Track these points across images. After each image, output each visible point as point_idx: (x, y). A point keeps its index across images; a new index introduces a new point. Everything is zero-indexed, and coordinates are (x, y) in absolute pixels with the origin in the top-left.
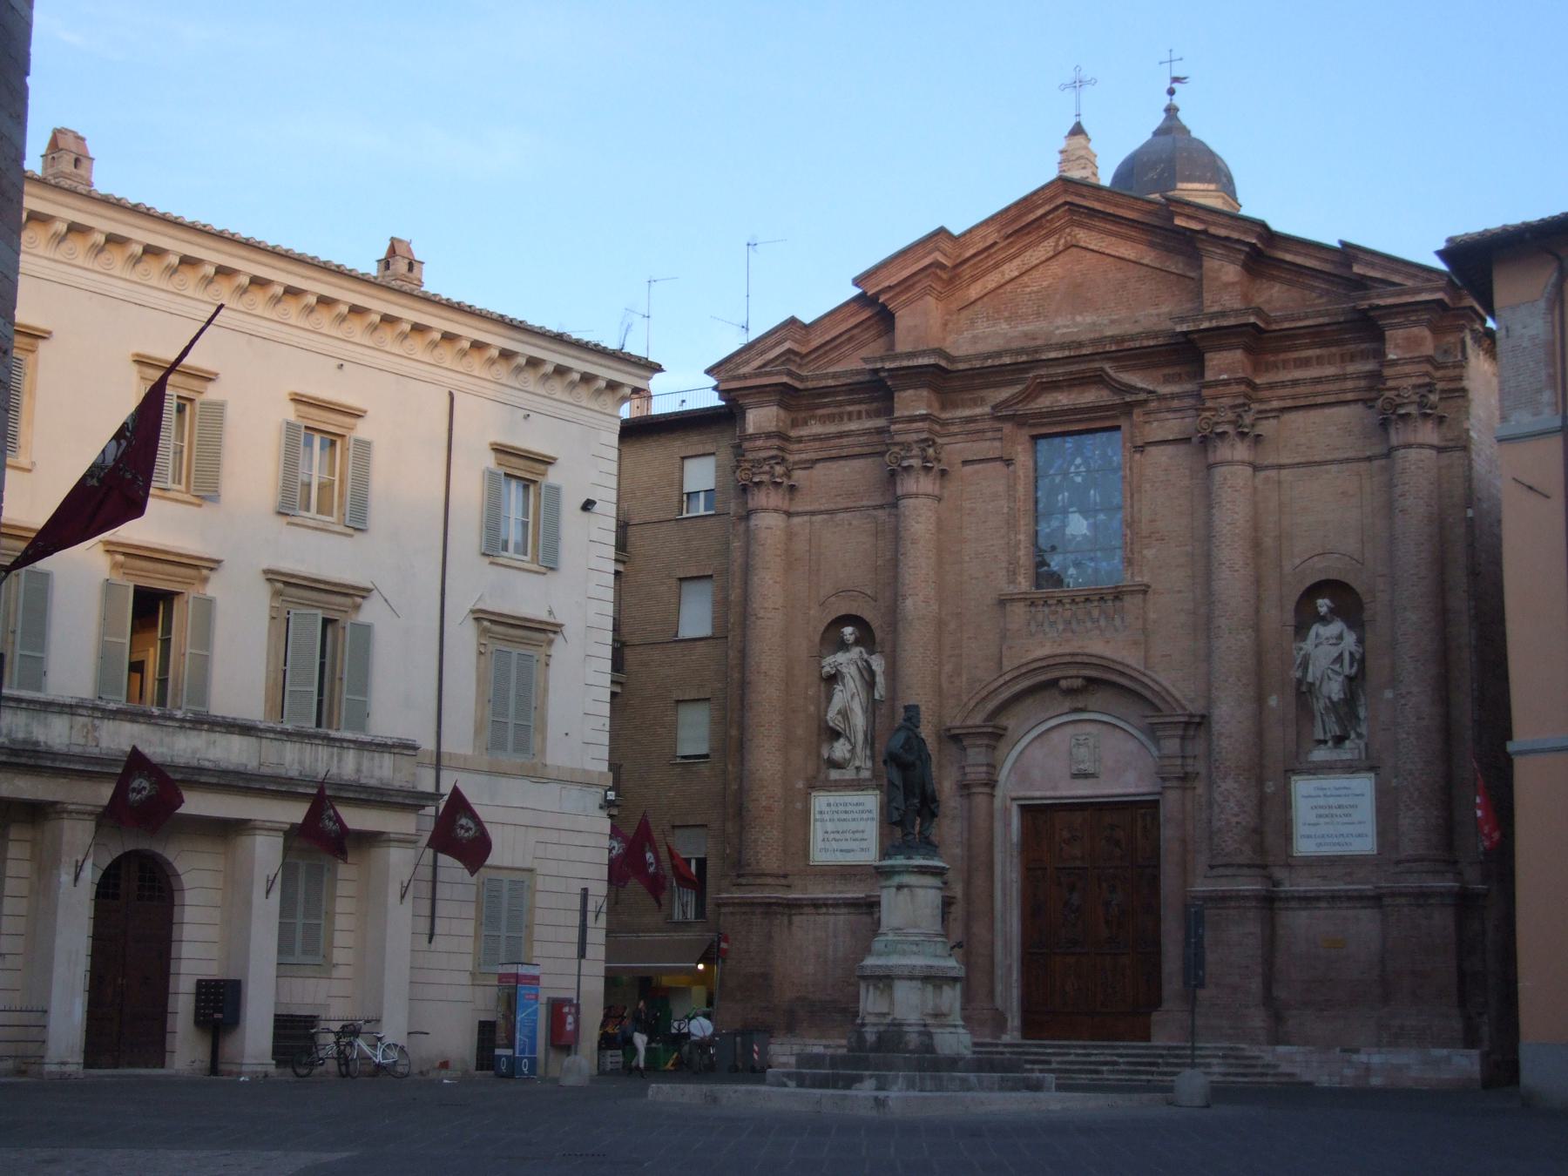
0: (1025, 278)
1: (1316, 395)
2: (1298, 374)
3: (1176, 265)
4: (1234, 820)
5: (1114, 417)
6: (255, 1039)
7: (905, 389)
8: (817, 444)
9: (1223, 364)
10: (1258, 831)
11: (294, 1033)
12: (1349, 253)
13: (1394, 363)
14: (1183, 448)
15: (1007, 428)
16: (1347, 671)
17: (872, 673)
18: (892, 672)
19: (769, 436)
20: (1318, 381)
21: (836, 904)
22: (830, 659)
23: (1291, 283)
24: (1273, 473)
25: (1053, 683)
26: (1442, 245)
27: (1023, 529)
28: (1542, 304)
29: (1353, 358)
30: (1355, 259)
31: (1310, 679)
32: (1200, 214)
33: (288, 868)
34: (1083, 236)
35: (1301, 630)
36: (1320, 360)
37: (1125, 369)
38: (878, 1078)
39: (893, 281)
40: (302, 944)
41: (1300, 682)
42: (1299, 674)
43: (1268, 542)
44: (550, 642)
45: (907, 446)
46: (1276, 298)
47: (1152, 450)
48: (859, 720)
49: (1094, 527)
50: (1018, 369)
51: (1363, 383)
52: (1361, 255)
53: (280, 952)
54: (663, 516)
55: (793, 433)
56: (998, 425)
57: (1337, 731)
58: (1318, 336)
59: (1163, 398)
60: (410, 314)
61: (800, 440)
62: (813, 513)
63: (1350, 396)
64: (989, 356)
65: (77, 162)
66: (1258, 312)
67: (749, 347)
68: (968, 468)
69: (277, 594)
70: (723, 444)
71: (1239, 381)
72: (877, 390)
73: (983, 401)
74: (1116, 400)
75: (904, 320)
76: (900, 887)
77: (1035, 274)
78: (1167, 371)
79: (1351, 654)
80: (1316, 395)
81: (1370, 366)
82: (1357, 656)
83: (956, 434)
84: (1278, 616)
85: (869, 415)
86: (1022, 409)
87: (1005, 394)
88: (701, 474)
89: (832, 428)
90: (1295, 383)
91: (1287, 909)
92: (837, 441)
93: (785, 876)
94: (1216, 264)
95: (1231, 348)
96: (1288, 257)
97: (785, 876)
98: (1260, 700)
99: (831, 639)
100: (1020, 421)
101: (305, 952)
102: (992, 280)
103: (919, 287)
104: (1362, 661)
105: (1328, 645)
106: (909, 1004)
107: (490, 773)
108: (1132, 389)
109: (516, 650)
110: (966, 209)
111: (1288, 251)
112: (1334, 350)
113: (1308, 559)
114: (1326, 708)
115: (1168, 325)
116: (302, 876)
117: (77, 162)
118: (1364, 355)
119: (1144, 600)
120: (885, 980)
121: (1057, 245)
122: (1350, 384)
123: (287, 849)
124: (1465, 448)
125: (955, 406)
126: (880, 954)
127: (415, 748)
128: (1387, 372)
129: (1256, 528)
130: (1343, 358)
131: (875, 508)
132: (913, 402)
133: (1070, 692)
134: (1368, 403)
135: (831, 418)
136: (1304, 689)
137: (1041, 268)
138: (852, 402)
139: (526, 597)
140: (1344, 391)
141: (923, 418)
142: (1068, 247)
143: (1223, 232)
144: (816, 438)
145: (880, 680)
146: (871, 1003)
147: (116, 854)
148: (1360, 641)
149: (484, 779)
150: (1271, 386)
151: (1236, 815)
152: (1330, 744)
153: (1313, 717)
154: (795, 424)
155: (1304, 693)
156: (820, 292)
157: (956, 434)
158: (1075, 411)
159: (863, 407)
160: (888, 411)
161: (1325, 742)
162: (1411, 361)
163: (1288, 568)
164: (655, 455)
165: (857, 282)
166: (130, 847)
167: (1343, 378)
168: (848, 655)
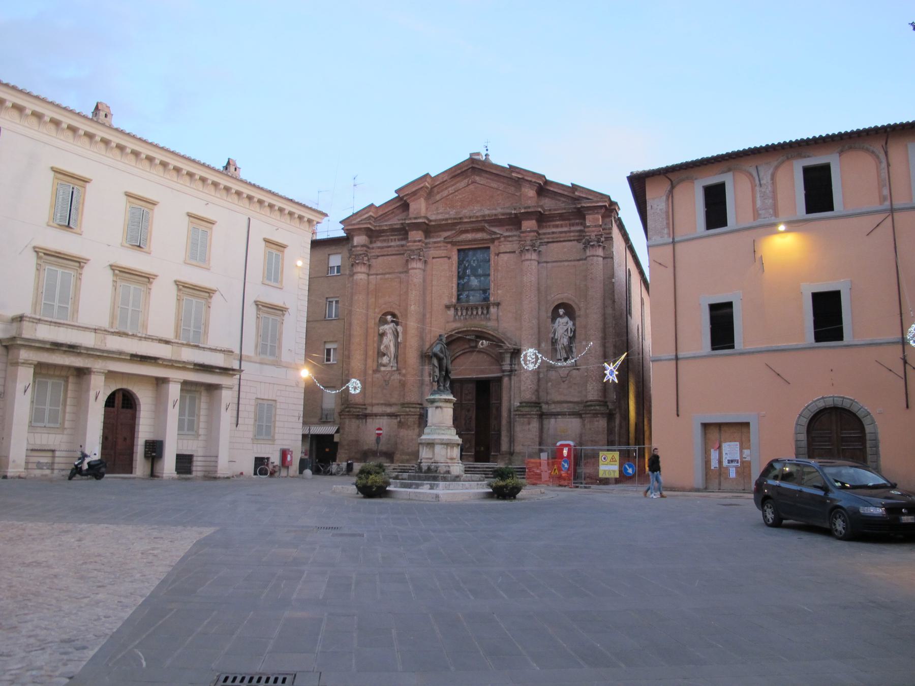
2: (554, 230)
3: (512, 190)
6: (169, 464)
9: (529, 225)
10: (537, 391)
11: (184, 462)
12: (574, 187)
13: (589, 227)
14: (512, 255)
15: (449, 246)
17: (398, 333)
18: (405, 332)
19: (362, 246)
20: (561, 232)
21: (382, 415)
22: (382, 328)
23: (552, 198)
24: (545, 265)
26: (629, 175)
28: (664, 198)
29: (573, 225)
30: (576, 190)
33: (182, 398)
34: (477, 178)
35: (553, 319)
36: (562, 226)
37: (493, 226)
38: (431, 485)
40: (187, 427)
44: (284, 315)
45: (412, 251)
46: (548, 204)
47: (502, 255)
48: (392, 349)
49: (480, 282)
50: (455, 224)
53: (179, 429)
55: (371, 246)
58: (562, 217)
59: (506, 237)
60: (235, 186)
61: (373, 248)
62: (377, 274)
65: (106, 116)
66: (542, 207)
67: (354, 215)
69: (179, 290)
70: (345, 250)
71: (533, 231)
72: (403, 231)
74: (488, 237)
75: (413, 206)
76: (437, 407)
81: (579, 228)
84: (547, 314)
85: (399, 240)
86: (455, 240)
88: (336, 260)
89: (385, 244)
90: (553, 233)
95: (532, 219)
99: (383, 321)
100: (453, 244)
101: (188, 430)
102: (445, 193)
105: (563, 325)
106: (440, 453)
107: (261, 363)
108: (495, 233)
109: (271, 317)
110: (437, 166)
113: (558, 297)
115: (508, 211)
116: (188, 401)
117: (106, 116)
118: (577, 224)
120: (431, 445)
122: (572, 234)
123: (182, 390)
124: (612, 258)
125: (430, 237)
126: (429, 434)
127: (232, 352)
128: (586, 230)
130: (570, 225)
131: (400, 273)
132: (416, 235)
134: (578, 241)
135: (385, 241)
139: (274, 297)
141: (419, 241)
142: (473, 182)
143: (529, 179)
144: (379, 248)
145: (400, 334)
146: (425, 453)
147: (114, 389)
148: (574, 324)
149: (257, 365)
150: (544, 234)
154: (371, 242)
155: (554, 342)
156: (384, 195)
158: (475, 240)
160: (406, 238)
162: (595, 226)
163: (549, 298)
164: (322, 252)
165: (396, 192)
166: (119, 387)
167: (570, 232)
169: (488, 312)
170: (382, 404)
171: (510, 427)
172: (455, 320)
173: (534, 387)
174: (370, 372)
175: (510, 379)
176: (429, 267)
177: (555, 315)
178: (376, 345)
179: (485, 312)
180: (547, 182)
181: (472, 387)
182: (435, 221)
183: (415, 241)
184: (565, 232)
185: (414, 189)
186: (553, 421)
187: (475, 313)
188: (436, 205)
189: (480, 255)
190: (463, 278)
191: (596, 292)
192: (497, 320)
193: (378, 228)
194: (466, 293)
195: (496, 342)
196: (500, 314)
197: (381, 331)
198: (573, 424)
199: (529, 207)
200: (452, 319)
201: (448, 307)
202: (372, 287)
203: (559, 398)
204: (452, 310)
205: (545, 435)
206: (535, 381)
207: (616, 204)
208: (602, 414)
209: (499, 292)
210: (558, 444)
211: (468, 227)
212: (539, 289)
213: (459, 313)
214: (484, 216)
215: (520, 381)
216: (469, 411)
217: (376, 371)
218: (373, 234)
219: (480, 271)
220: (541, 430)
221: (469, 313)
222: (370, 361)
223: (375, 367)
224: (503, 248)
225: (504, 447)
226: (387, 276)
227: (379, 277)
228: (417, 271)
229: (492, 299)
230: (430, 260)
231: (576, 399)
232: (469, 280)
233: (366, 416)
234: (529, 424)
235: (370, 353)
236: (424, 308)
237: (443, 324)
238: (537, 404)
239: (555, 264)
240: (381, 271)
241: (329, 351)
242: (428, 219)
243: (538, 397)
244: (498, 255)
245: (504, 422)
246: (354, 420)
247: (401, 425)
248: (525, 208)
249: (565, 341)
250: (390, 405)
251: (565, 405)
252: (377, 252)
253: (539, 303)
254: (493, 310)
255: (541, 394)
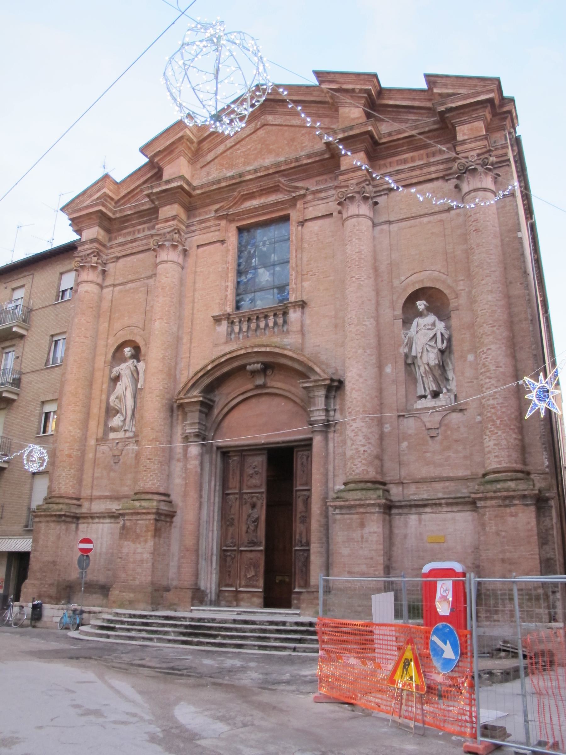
0: (238, 146)
1: (412, 177)
4: (362, 449)
5: (286, 209)
7: (165, 205)
8: (120, 248)
10: (379, 457)
13: (463, 142)
14: (327, 221)
15: (223, 223)
16: (440, 345)
20: (412, 169)
21: (102, 516)
24: (385, 227)
25: (242, 368)
27: (230, 279)
31: (413, 354)
32: (337, 78)
35: (407, 323)
36: (413, 159)
39: (162, 148)
41: (406, 356)
42: (406, 350)
43: (383, 268)
47: (308, 224)
48: (130, 402)
49: (274, 274)
51: (441, 167)
52: (439, 80)
54: (47, 304)
56: (217, 222)
57: (434, 387)
59: (314, 193)
62: (114, 285)
63: (434, 176)
64: (214, 183)
68: (201, 250)
73: (210, 211)
77: (243, 143)
78: (318, 178)
79: (442, 334)
80: (412, 177)
82: (446, 336)
83: (194, 231)
84: (392, 312)
87: (217, 206)
91: (400, 514)
92: (130, 245)
93: (78, 499)
94: (347, 110)
96: (391, 102)
97: (78, 499)
98: (380, 367)
103: (177, 151)
104: (449, 340)
105: (425, 331)
111: (390, 99)
112: (421, 152)
114: (425, 372)
119: (303, 313)
121: (256, 125)
122: (433, 169)
125: (195, 216)
129: (375, 259)
133: (254, 373)
135: (129, 234)
136: (409, 361)
137: (247, 139)
138: (140, 224)
140: (429, 173)
143: (350, 87)
144: (120, 245)
145: (141, 375)
148: (448, 328)
151: (364, 446)
152: (429, 397)
153: (415, 381)
155: (410, 364)
156: (126, 163)
157: (194, 231)
159: (146, 226)
161: (425, 397)
163: (396, 283)
165: (143, 150)
167: (428, 165)
168: (126, 364)
169: (285, 322)
170: (106, 497)
171: (328, 538)
172: (228, 341)
173: (372, 449)
174: (92, 442)
175: (326, 439)
176: (191, 260)
177: (409, 310)
178: (104, 397)
179: (280, 321)
180: (381, 92)
181: (259, 462)
182: (202, 187)
183: (167, 220)
184: (420, 167)
185: (168, 143)
186: (413, 519)
187: (262, 324)
188: (206, 169)
189: (273, 232)
190: (246, 273)
191: (488, 253)
192: (302, 332)
193: (118, 215)
194: (250, 296)
195: (298, 371)
196: (308, 322)
197: (113, 375)
198: (458, 525)
199: (351, 128)
200: (223, 340)
201: (217, 320)
202: (106, 305)
203: (425, 472)
204: (225, 323)
205: (397, 551)
206: (374, 439)
207: (512, 100)
208: (524, 497)
209: (306, 284)
210: (426, 569)
211: (253, 188)
212: (376, 269)
213: (237, 329)
214: (278, 164)
215: (344, 442)
216: (253, 506)
217: (102, 440)
218: (110, 224)
219: (274, 258)
220: (389, 539)
221: (253, 326)
222: (93, 424)
223: (100, 435)
224: (311, 212)
225: (317, 576)
226: (129, 286)
227: (117, 288)
228: (169, 265)
229: (292, 298)
230: (193, 251)
231: (460, 473)
232: (255, 275)
233: (77, 518)
234: (362, 525)
235: (95, 410)
236: (180, 327)
237: (208, 346)
238: (380, 484)
239: (403, 224)
240: (121, 280)
241: (47, 415)
242: (189, 184)
243: (381, 470)
244: (302, 223)
245: (315, 524)
246: (52, 525)
247: (125, 533)
248: (344, 131)
249: (432, 358)
250: (117, 498)
251: (439, 486)
252: (117, 252)
253: (378, 292)
254: (294, 315)
255: (388, 465)
